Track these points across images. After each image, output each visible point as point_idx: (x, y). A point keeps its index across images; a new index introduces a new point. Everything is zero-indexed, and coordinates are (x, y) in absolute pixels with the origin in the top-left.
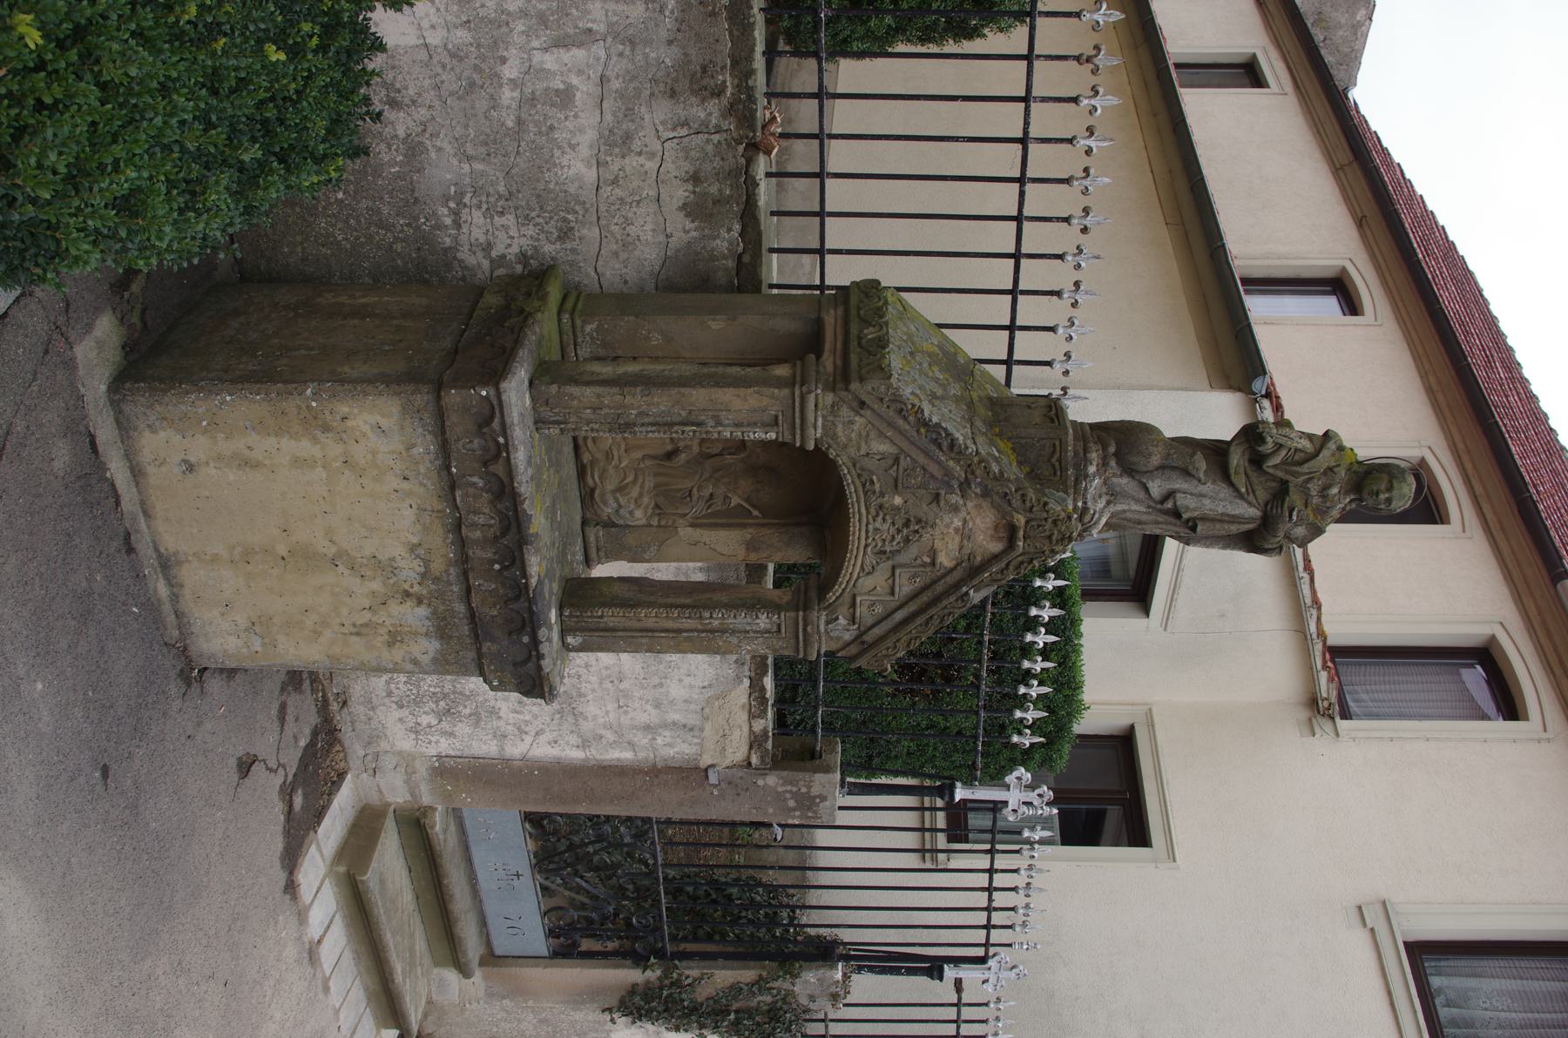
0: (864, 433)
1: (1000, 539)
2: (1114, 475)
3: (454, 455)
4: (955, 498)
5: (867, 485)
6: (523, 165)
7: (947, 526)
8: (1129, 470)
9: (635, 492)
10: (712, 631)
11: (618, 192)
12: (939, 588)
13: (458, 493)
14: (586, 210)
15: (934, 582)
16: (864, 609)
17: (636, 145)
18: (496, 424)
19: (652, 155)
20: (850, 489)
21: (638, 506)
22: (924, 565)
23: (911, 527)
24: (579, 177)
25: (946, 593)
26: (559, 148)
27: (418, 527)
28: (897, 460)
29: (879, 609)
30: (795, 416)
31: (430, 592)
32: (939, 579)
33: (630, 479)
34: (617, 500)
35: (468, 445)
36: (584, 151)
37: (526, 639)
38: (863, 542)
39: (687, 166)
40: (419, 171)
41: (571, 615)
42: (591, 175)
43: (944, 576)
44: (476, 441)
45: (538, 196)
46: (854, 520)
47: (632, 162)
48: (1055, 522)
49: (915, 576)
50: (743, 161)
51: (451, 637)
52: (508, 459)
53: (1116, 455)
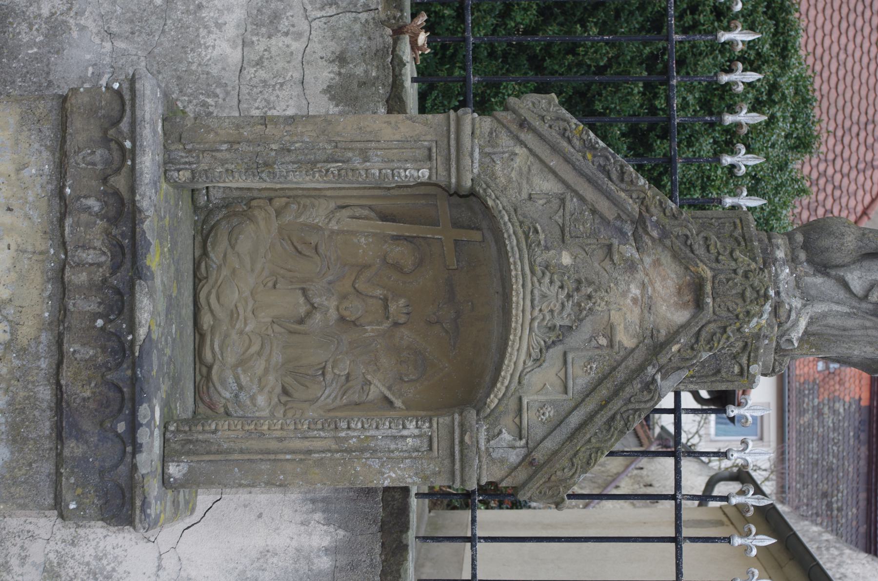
0: (525, 169)
1: (685, 305)
2: (807, 274)
3: (71, 171)
4: (629, 251)
5: (529, 231)
6: (167, 45)
7: (624, 294)
8: (823, 268)
9: (260, 366)
10: (349, 451)
11: (262, 74)
12: (621, 375)
13: (68, 222)
14: (227, 93)
15: (614, 369)
17: (284, 25)
18: (124, 125)
19: (298, 36)
21: (261, 389)
22: (600, 347)
23: (581, 290)
24: (223, 58)
25: (629, 380)
26: (206, 27)
27: (13, 275)
28: (563, 201)
29: (550, 412)
30: (454, 153)
31: (11, 372)
33: (255, 348)
34: (237, 379)
35: (88, 157)
36: (231, 31)
37: (121, 427)
38: (528, 317)
39: (334, 47)
40: (57, 52)
41: (178, 431)
42: (235, 56)
43: (624, 359)
44: (99, 152)
45: (179, 78)
47: (278, 43)
48: (746, 275)
49: (591, 360)
50: (391, 41)
51: (25, 440)
52: (133, 168)
53: (805, 247)
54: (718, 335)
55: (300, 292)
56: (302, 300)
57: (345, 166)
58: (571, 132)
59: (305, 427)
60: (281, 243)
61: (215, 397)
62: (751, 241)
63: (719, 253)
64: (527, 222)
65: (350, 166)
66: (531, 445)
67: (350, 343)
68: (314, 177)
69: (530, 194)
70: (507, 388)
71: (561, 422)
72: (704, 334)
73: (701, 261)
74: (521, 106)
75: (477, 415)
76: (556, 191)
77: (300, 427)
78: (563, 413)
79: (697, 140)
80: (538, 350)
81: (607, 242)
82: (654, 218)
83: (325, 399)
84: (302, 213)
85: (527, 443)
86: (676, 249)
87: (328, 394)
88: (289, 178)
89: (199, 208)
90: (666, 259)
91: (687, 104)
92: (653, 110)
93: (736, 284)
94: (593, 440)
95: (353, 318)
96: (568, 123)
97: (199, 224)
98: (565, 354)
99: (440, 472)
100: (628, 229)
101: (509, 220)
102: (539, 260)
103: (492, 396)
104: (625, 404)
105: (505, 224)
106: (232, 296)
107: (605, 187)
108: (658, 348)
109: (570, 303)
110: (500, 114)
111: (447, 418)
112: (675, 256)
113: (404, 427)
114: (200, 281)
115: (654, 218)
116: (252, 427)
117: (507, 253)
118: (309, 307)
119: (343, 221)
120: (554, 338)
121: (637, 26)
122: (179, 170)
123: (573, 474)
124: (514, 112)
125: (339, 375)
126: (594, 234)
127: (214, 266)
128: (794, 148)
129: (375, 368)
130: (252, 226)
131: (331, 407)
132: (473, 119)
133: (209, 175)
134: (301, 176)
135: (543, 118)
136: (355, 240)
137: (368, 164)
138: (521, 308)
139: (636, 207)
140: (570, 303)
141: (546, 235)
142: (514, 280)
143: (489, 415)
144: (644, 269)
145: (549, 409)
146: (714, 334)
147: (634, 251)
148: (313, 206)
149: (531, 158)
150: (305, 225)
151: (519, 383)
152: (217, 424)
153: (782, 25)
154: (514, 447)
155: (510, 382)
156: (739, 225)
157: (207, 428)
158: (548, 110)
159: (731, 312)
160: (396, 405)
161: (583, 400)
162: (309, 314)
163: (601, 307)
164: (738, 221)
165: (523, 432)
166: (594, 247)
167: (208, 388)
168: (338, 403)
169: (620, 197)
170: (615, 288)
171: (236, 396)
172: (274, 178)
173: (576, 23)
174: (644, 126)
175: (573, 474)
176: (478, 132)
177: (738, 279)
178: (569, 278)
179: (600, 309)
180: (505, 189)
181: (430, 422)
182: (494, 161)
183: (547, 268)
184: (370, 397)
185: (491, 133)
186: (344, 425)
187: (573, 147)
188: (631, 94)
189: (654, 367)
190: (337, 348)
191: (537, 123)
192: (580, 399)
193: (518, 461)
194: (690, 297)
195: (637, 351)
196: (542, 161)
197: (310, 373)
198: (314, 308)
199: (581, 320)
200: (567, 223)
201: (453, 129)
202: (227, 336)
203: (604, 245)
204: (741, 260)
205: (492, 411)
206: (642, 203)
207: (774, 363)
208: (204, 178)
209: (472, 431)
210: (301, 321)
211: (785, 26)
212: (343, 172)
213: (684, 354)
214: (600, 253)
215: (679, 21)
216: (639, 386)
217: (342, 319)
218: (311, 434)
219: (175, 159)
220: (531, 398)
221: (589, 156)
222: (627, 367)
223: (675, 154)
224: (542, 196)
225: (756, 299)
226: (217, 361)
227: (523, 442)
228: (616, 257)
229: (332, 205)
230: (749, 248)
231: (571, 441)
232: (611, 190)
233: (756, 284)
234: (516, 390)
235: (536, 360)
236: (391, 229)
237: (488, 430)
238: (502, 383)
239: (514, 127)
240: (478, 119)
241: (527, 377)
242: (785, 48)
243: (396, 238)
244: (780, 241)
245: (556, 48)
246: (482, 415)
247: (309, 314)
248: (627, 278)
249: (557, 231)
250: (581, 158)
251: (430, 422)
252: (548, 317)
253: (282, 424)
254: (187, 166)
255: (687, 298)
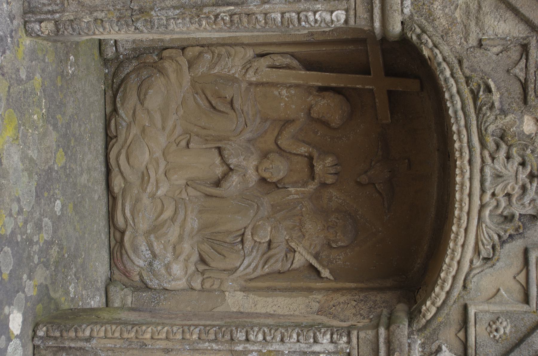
9: (173, 233)
16: (482, 328)
28: (525, 48)
29: (505, 328)
33: (168, 213)
38: (477, 202)
41: (48, 337)
46: (462, 162)
55: (216, 152)
56: (218, 160)
57: (238, 10)
59: (195, 336)
60: (195, 98)
61: (129, 265)
64: (476, 79)
65: (244, 9)
67: (272, 205)
68: (200, 25)
69: (480, 40)
70: (448, 293)
71: (521, 341)
75: (410, 325)
77: (188, 336)
78: (523, 329)
80: (489, 247)
83: (245, 269)
84: (216, 64)
87: (249, 263)
88: (171, 27)
89: (108, 60)
95: (275, 180)
97: (110, 78)
98: (526, 252)
101: (452, 75)
102: (491, 128)
103: (428, 303)
105: (446, 80)
106: (142, 157)
113: (316, 341)
114: (111, 139)
116: (133, 335)
118: (225, 168)
119: (262, 70)
120: (511, 231)
122: (41, 21)
125: (260, 243)
127: (124, 124)
129: (300, 234)
130: (162, 79)
131: (253, 276)
133: (75, 26)
134: (184, 24)
136: (276, 93)
137: (267, 6)
141: (502, 95)
142: (457, 154)
143: (425, 327)
145: (505, 324)
148: (229, 55)
150: (220, 77)
151: (465, 287)
152: (92, 330)
155: (452, 286)
157: (80, 334)
160: (323, 275)
162: (225, 176)
167: (121, 254)
168: (259, 272)
171: (151, 264)
172: (152, 28)
180: (447, 34)
181: (349, 335)
183: (502, 138)
184: (296, 265)
186: (241, 336)
190: (256, 214)
197: (228, 240)
198: (231, 170)
200: (532, 78)
202: (138, 200)
205: (429, 322)
208: (70, 30)
210: (218, 184)
212: (236, 18)
217: (263, 180)
218: (201, 346)
219: (37, 7)
220: (481, 308)
224: (497, 42)
226: (129, 227)
229: (250, 53)
235: (487, 259)
236: (317, 79)
237: (423, 345)
238: (442, 288)
241: (475, 279)
243: (322, 89)
246: (415, 327)
247: (225, 176)
249: (517, 89)
251: (349, 335)
252: (503, 204)
253: (167, 332)
254: (49, 16)
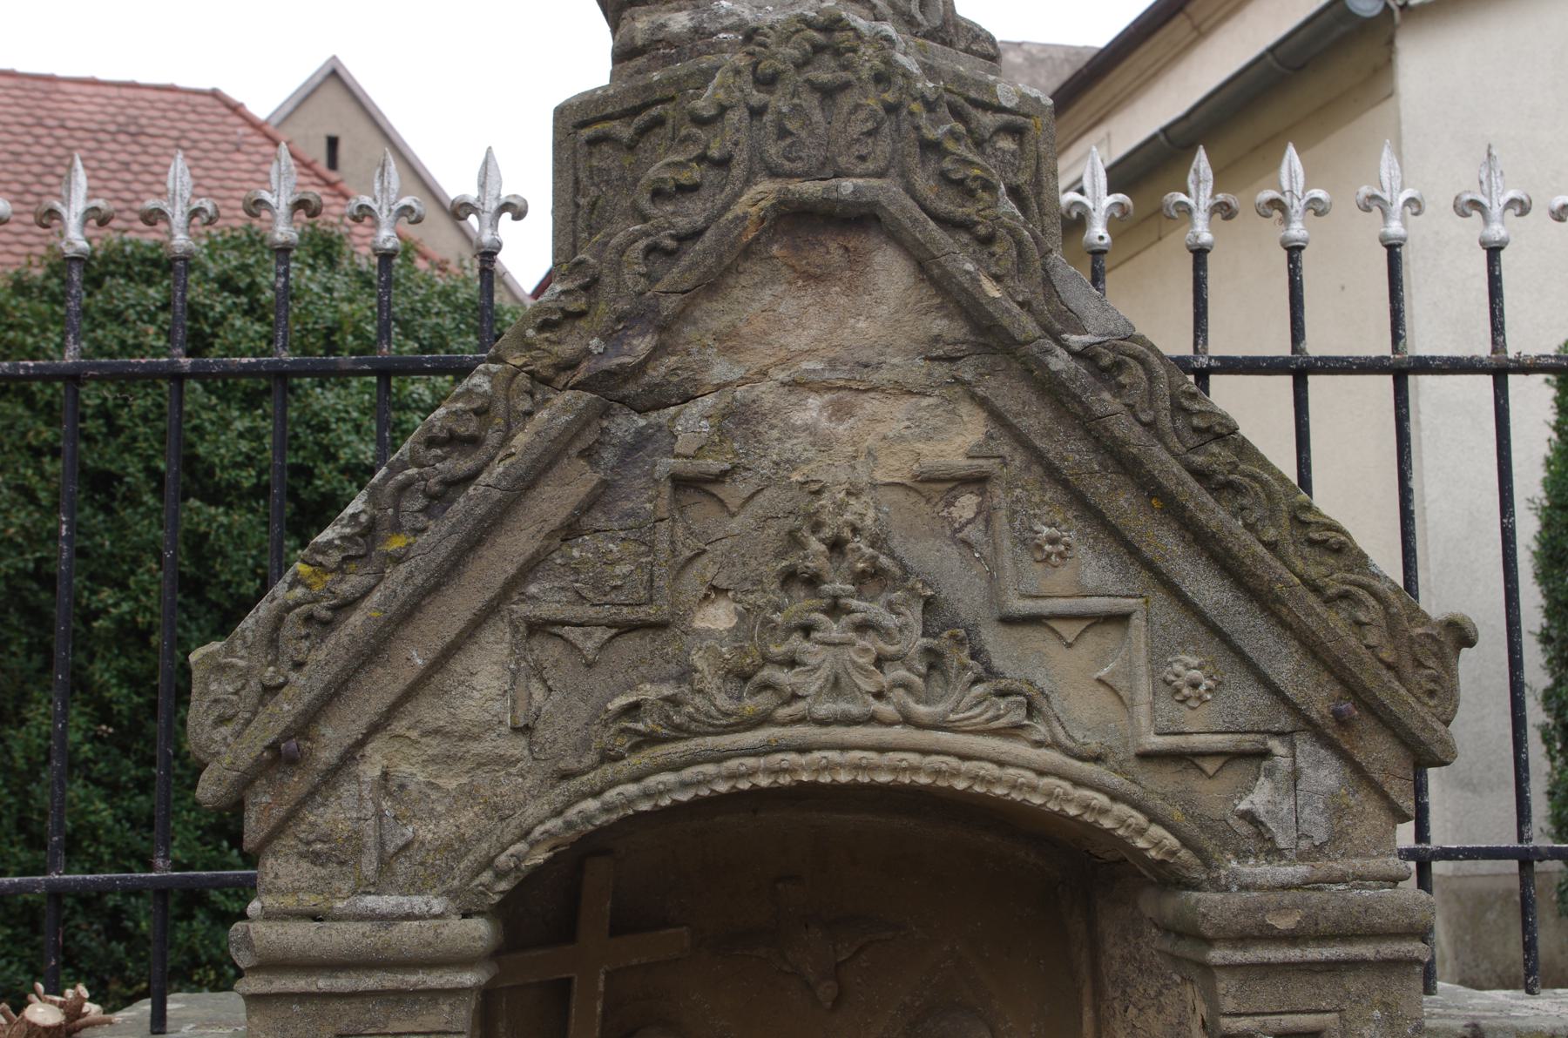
0: (434, 746)
1: (855, 260)
4: (692, 423)
7: (825, 444)
12: (1073, 453)
15: (1053, 473)
16: (1194, 718)
20: (671, 787)
22: (986, 515)
23: (823, 567)
28: (538, 628)
29: (1188, 665)
32: (1037, 456)
43: (1021, 440)
46: (804, 769)
48: (767, 82)
54: (947, 164)
58: (316, 600)
62: (648, 87)
63: (702, 158)
66: (1284, 722)
69: (515, 730)
70: (1115, 797)
72: (945, 206)
73: (726, 208)
74: (227, 760)
75: (1197, 887)
76: (504, 649)
79: (316, 414)
80: (1002, 703)
81: (666, 490)
82: (595, 344)
85: (1279, 734)
86: (691, 279)
90: (716, 316)
91: (250, 430)
92: (260, 491)
93: (795, 108)
94: (1271, 534)
96: (289, 609)
98: (1009, 621)
99: (1386, 1005)
100: (626, 425)
101: (596, 794)
103: (1141, 843)
104: (1161, 439)
107: (497, 494)
108: (989, 336)
109: (854, 603)
110: (254, 827)
111: (1221, 986)
112: (711, 285)
115: (595, 344)
117: (697, 802)
121: (101, 517)
123: (1374, 594)
124: (247, 782)
126: (641, 532)
128: (332, 264)
132: (269, 916)
135: (271, 690)
138: (873, 756)
139: (558, 400)
140: (854, 603)
142: (785, 780)
143: (1198, 851)
144: (744, 381)
145: (1178, 668)
146: (944, 176)
147: (694, 408)
149: (399, 726)
151: (1097, 759)
153: (112, 267)
154: (1295, 775)
156: (600, 127)
158: (245, 674)
159: (880, 124)
161: (1149, 565)
163: (863, 510)
164: (586, 133)
165: (1247, 746)
166: (679, 531)
169: (528, 448)
170: (806, 469)
173: (90, 629)
174: (289, 508)
175: (1374, 594)
176: (310, 901)
177: (779, 102)
178: (778, 608)
179: (871, 514)
180: (496, 808)
182: (407, 846)
183: (745, 677)
185: (315, 859)
187: (367, 592)
188: (228, 529)
189: (1048, 352)
191: (286, 709)
192: (1145, 574)
193: (1335, 763)
194: (833, 246)
195: (999, 403)
196: (409, 694)
199: (906, 571)
200: (606, 612)
201: (299, 984)
203: (675, 500)
204: (721, 95)
205: (1185, 843)
206: (547, 382)
207: (974, 53)
209: (1261, 908)
211: (115, 262)
213: (1007, 264)
214: (701, 513)
215: (96, 442)
216: (1106, 396)
220: (1144, 722)
221: (396, 544)
222: (1049, 434)
223: (370, 362)
225: (837, 53)
227: (1275, 745)
228: (713, 464)
230: (672, 91)
231: (1278, 600)
232: (505, 474)
233: (796, 53)
234: (1120, 770)
235: (1031, 709)
237: (1242, 855)
238: (1104, 812)
239: (297, 784)
240: (269, 901)
241: (1078, 735)
242: (156, 263)
244: (639, 25)
245: (137, 664)
246: (1199, 874)
248: (775, 433)
249: (632, 645)
250: (403, 569)
255: (836, 255)
